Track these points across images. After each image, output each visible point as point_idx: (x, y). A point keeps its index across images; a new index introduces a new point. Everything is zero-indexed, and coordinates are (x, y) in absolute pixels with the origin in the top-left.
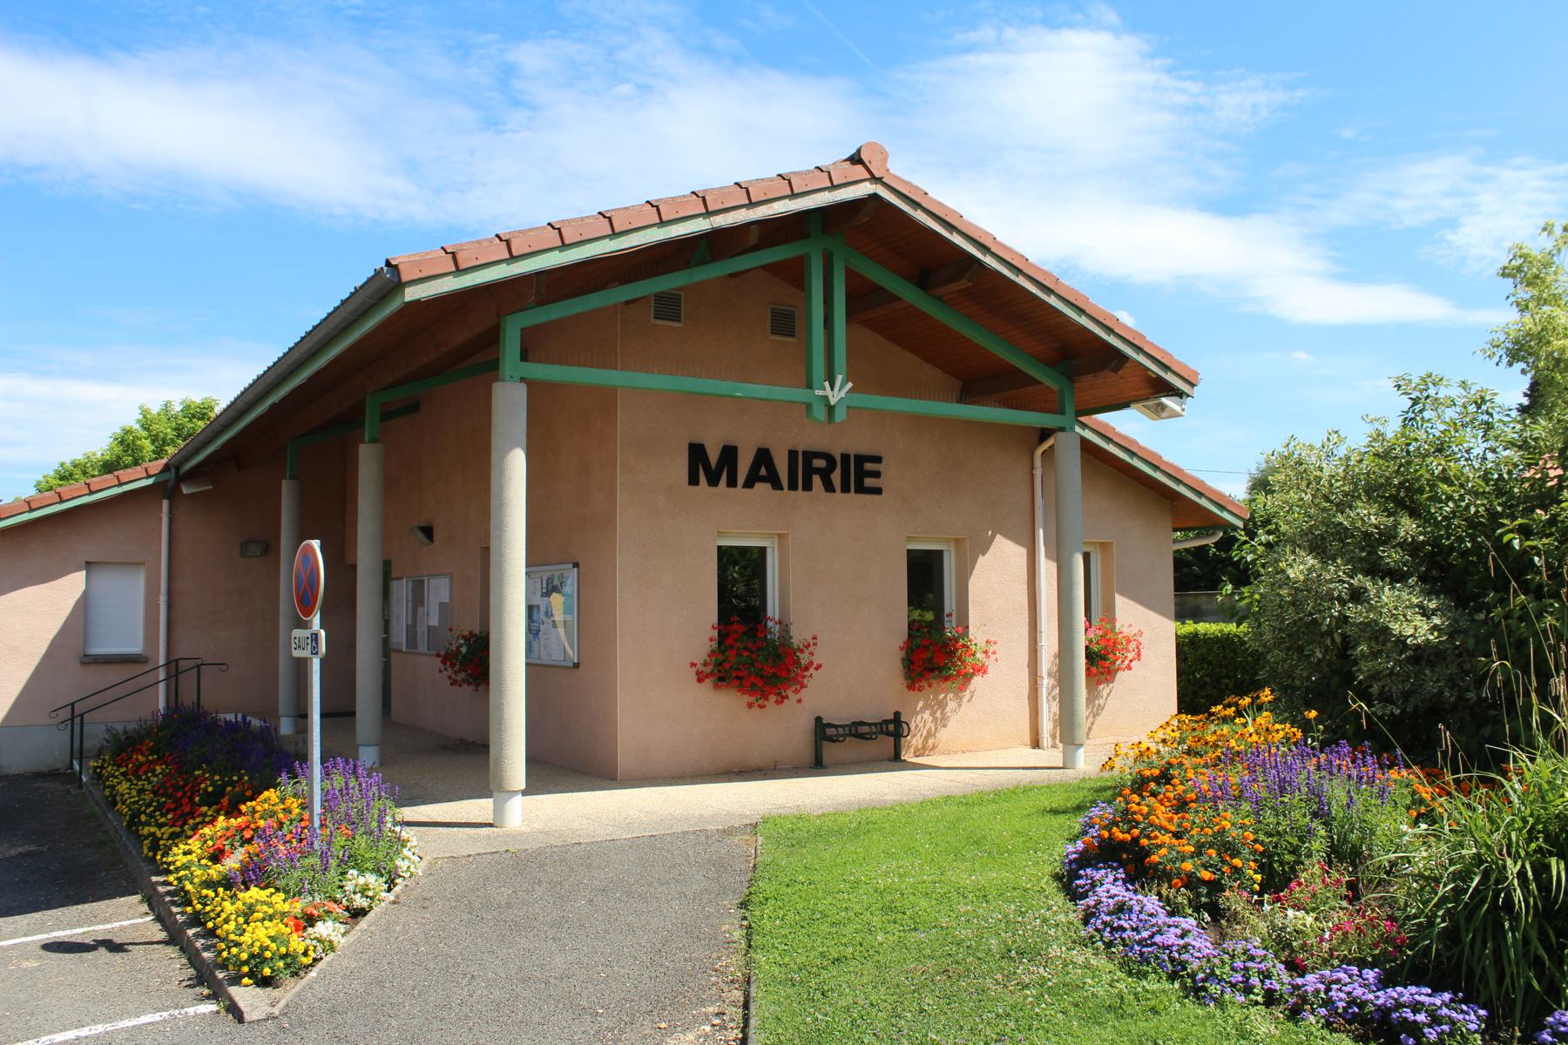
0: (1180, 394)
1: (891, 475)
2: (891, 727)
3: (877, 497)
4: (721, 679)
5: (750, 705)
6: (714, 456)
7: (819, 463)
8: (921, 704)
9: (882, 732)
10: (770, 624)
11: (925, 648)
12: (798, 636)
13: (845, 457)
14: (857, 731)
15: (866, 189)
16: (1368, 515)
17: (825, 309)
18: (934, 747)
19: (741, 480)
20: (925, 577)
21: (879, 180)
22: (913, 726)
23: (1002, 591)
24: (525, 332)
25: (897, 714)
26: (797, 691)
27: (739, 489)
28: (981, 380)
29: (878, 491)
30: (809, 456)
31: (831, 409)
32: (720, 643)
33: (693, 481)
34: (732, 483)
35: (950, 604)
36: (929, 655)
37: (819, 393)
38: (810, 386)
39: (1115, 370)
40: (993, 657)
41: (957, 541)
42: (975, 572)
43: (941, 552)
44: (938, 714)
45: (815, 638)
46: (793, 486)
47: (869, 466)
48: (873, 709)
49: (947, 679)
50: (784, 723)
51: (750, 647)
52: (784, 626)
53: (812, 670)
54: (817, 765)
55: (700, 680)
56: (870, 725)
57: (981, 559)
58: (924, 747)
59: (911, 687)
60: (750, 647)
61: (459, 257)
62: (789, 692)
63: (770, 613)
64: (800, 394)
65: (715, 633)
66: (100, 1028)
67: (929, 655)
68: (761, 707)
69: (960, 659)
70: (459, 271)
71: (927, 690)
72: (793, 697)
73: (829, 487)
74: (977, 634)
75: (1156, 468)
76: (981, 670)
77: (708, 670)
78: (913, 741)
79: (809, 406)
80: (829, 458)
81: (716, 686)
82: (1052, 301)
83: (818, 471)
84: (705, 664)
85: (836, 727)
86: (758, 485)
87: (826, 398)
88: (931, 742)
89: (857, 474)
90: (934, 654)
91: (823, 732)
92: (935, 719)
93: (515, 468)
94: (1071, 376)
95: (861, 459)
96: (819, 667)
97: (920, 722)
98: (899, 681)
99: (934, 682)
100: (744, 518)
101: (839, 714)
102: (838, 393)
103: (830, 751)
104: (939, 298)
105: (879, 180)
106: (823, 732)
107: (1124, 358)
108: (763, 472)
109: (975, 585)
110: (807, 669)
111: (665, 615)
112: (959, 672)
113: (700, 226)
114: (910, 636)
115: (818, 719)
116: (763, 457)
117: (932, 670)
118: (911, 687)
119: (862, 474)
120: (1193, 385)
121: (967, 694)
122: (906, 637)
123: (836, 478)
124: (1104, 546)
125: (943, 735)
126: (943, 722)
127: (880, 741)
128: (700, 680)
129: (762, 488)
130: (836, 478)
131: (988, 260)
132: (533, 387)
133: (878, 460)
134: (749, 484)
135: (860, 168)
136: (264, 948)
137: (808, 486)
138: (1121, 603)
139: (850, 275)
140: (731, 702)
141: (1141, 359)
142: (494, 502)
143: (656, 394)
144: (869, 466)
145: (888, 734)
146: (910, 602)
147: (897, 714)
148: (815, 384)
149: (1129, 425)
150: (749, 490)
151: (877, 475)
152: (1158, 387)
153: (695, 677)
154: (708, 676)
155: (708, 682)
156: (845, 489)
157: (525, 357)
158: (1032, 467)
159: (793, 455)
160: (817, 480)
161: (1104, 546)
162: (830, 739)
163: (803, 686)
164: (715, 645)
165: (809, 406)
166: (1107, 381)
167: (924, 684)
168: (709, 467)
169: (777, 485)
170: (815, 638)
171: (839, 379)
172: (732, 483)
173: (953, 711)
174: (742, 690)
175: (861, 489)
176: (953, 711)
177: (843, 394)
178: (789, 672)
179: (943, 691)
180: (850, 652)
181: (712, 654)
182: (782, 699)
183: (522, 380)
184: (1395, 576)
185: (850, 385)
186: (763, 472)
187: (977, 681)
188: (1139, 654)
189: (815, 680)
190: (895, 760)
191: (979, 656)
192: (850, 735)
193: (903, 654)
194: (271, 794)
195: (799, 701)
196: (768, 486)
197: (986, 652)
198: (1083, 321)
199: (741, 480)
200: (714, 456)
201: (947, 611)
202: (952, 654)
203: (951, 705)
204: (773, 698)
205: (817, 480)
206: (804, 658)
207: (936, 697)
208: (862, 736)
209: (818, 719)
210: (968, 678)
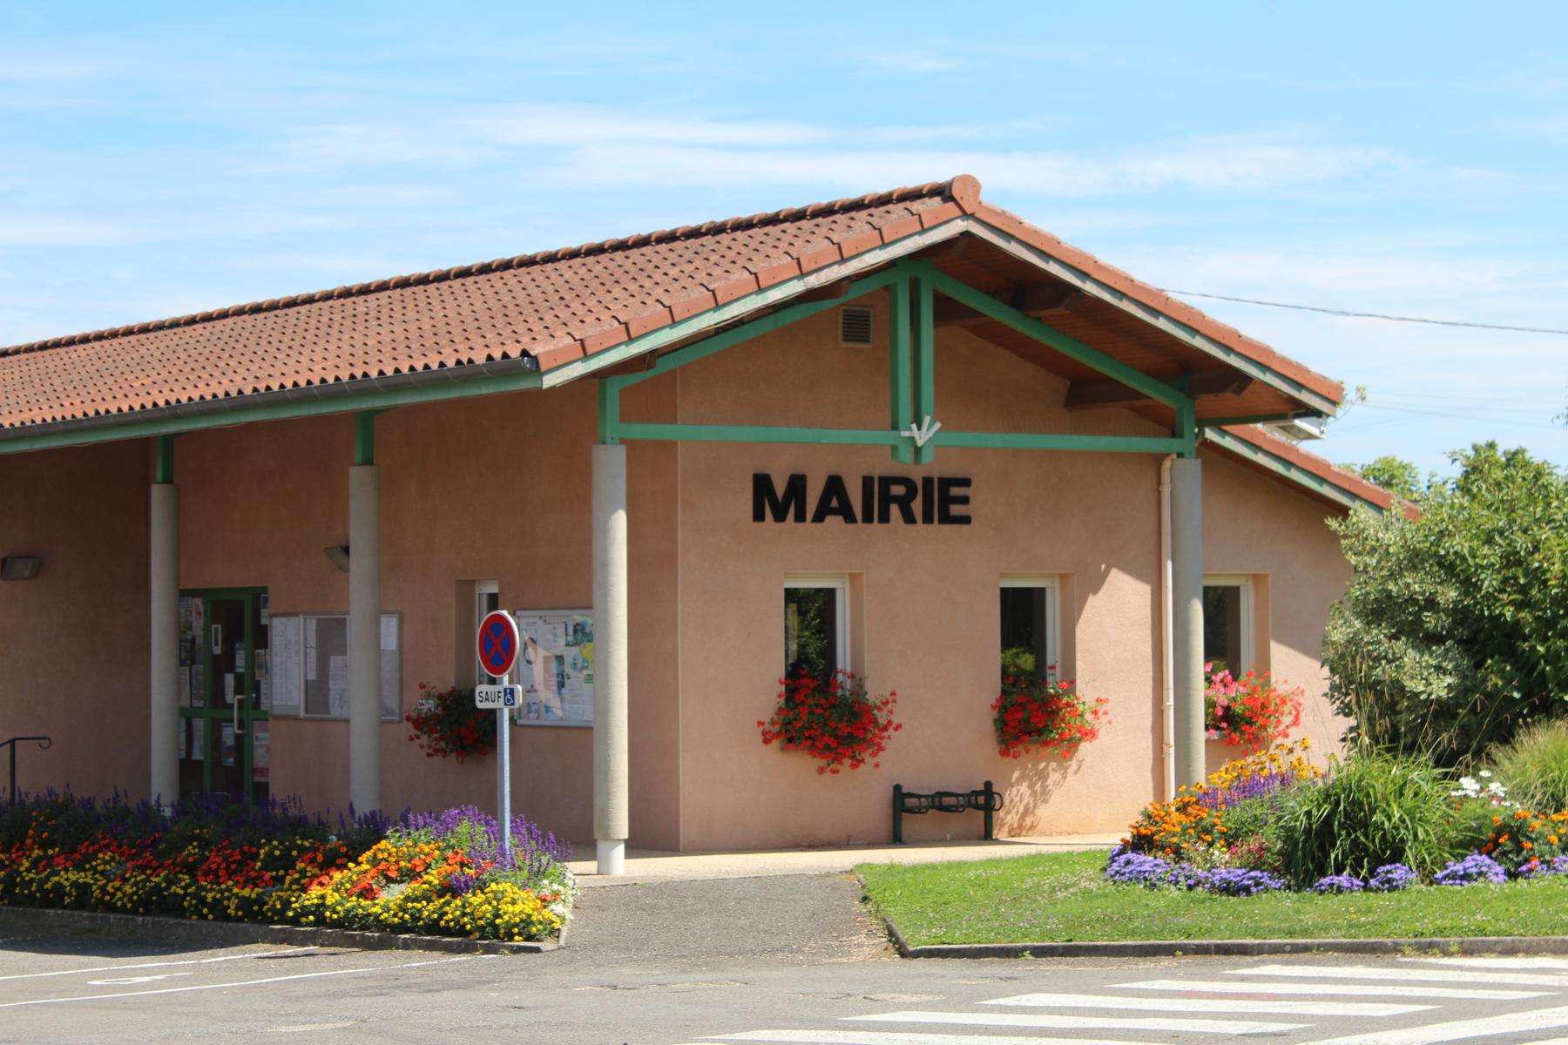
0: (1318, 414)
1: (981, 501)
2: (981, 799)
3: (964, 527)
4: (790, 740)
5: (821, 770)
6: (780, 488)
7: (897, 490)
8: (1016, 775)
9: (970, 805)
10: (840, 677)
11: (1022, 707)
12: (874, 692)
13: (928, 481)
14: (941, 802)
15: (957, 227)
16: (1415, 584)
17: (917, 346)
18: (1032, 827)
19: (810, 514)
20: (1023, 617)
21: (972, 216)
22: (1007, 800)
23: (1116, 635)
24: (623, 393)
25: (988, 785)
26: (874, 755)
27: (808, 526)
28: (1084, 395)
29: (966, 520)
30: (886, 482)
31: (918, 451)
32: (787, 701)
33: (759, 516)
34: (800, 517)
35: (1053, 654)
36: (1026, 714)
37: (905, 434)
38: (895, 427)
39: (1238, 392)
40: (1104, 719)
41: (1064, 578)
42: (1084, 614)
43: (1042, 591)
44: (1038, 787)
45: (893, 694)
46: (868, 519)
47: (955, 491)
48: (962, 777)
49: (1046, 744)
50: (863, 787)
51: (822, 710)
52: (857, 679)
53: (891, 731)
54: (896, 839)
55: (766, 741)
56: (957, 795)
57: (1093, 602)
58: (1020, 827)
59: (1004, 753)
60: (822, 710)
61: (587, 344)
62: (866, 755)
63: (840, 666)
64: (884, 437)
65: (783, 688)
66: (301, 1028)
67: (1026, 714)
68: (835, 772)
69: (1063, 720)
70: (586, 356)
71: (1023, 757)
72: (870, 761)
73: (909, 518)
74: (1086, 690)
75: (1322, 480)
76: (1091, 734)
77: (775, 729)
78: (1006, 817)
79: (894, 448)
80: (907, 482)
81: (783, 749)
82: (1162, 324)
83: (897, 499)
84: (773, 723)
85: (919, 797)
86: (829, 519)
87: (912, 439)
88: (1028, 820)
89: (941, 500)
90: (1032, 712)
91: (901, 802)
92: (1034, 793)
93: (620, 521)
94: (1191, 392)
95: (946, 483)
96: (898, 727)
97: (1016, 796)
98: (990, 745)
99: (1033, 748)
100: (812, 555)
101: (921, 781)
102: (922, 437)
103: (910, 824)
104: (1039, 319)
105: (972, 216)
106: (901, 802)
107: (1248, 379)
108: (834, 503)
109: (1085, 631)
110: (885, 729)
111: (742, 667)
112: (1062, 739)
113: (796, 288)
114: (1004, 692)
115: (897, 788)
116: (835, 485)
117: (1030, 734)
118: (1004, 753)
119: (947, 500)
120: (1334, 403)
121: (1074, 764)
122: (999, 694)
123: (917, 506)
124: (1258, 579)
125: (1044, 812)
126: (1044, 795)
127: (973, 813)
128: (766, 741)
129: (834, 522)
130: (917, 506)
131: (1089, 288)
132: (634, 449)
133: (966, 482)
134: (819, 517)
135: (951, 204)
136: (530, 916)
137: (885, 518)
138: (1278, 652)
139: (941, 301)
140: (799, 767)
141: (1269, 378)
142: (596, 563)
143: (731, 439)
144: (955, 491)
145: (977, 807)
146: (1006, 644)
147: (988, 785)
148: (902, 424)
149: (1257, 442)
150: (818, 525)
151: (965, 500)
152: (1296, 403)
153: (761, 738)
154: (775, 736)
155: (776, 743)
156: (928, 519)
157: (625, 418)
158: (1159, 483)
159: (867, 482)
160: (895, 510)
161: (1258, 579)
162: (911, 811)
163: (881, 748)
164: (782, 701)
165: (894, 448)
166: (1228, 401)
167: (1021, 748)
168: (776, 500)
169: (849, 517)
170: (893, 694)
171: (927, 420)
172: (800, 517)
173: (1057, 784)
174: (814, 751)
175: (946, 519)
176: (1057, 784)
177: (931, 434)
178: (865, 731)
179: (1043, 758)
180: (935, 709)
181: (780, 711)
182: (857, 762)
183: (623, 441)
184: (1429, 640)
185: (938, 425)
186: (834, 503)
187: (1085, 748)
188: (1297, 718)
189: (894, 743)
190: (987, 837)
191: (1089, 717)
192: (934, 807)
193: (995, 713)
194: (383, 844)
195: (877, 765)
196: (840, 519)
197: (1095, 712)
198: (1198, 342)
199: (810, 514)
200: (780, 488)
201: (1050, 662)
202: (1054, 714)
203: (1054, 776)
204: (847, 762)
205: (895, 510)
206: (882, 716)
207: (1035, 767)
208: (947, 809)
209: (897, 788)
210: (1073, 744)
